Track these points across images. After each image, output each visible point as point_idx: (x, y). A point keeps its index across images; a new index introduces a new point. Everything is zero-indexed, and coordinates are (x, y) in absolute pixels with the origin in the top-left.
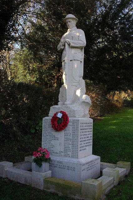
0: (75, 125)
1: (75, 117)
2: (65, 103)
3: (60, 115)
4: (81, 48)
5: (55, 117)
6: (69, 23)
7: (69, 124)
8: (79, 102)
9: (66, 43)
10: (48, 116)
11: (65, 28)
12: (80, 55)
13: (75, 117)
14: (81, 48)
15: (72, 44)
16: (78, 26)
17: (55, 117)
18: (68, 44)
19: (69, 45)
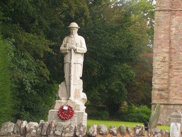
0: (80, 117)
1: (79, 110)
2: (70, 98)
3: (66, 108)
4: (155, 89)
5: (62, 110)
6: (73, 31)
7: (74, 115)
8: (79, 98)
9: (72, 49)
10: (54, 109)
11: (68, 33)
12: (81, 60)
13: (79, 110)
14: (82, 54)
15: (78, 51)
16: (80, 33)
17: (62, 110)
18: (74, 50)
19: (75, 50)
